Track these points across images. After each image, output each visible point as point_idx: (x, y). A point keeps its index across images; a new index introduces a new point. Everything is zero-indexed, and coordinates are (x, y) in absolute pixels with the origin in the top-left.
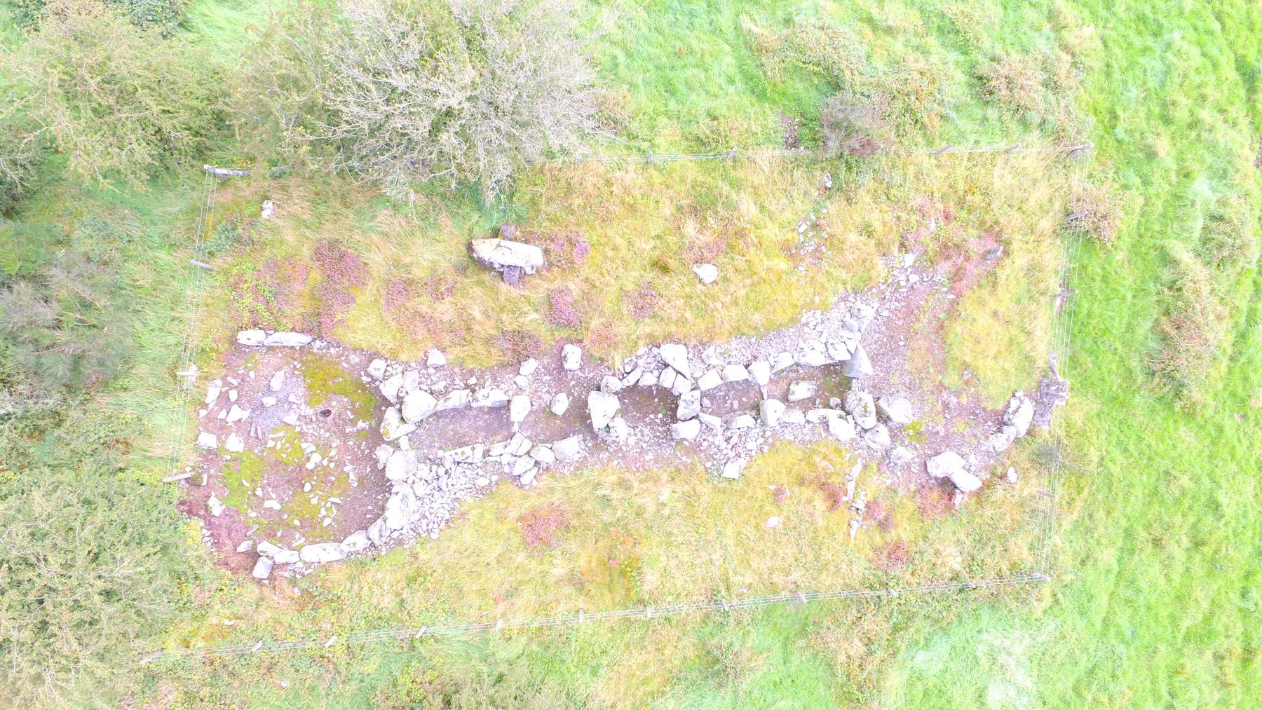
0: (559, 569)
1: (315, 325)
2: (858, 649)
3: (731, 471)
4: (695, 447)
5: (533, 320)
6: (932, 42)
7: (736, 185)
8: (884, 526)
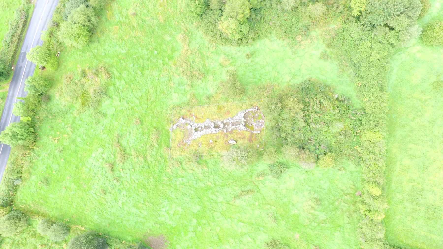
0: (226, 109)
1: (252, 134)
2: (193, 101)
3: (208, 119)
4: (212, 122)
5: (230, 135)
6: (186, 169)
7: (208, 151)
8: (190, 114)
